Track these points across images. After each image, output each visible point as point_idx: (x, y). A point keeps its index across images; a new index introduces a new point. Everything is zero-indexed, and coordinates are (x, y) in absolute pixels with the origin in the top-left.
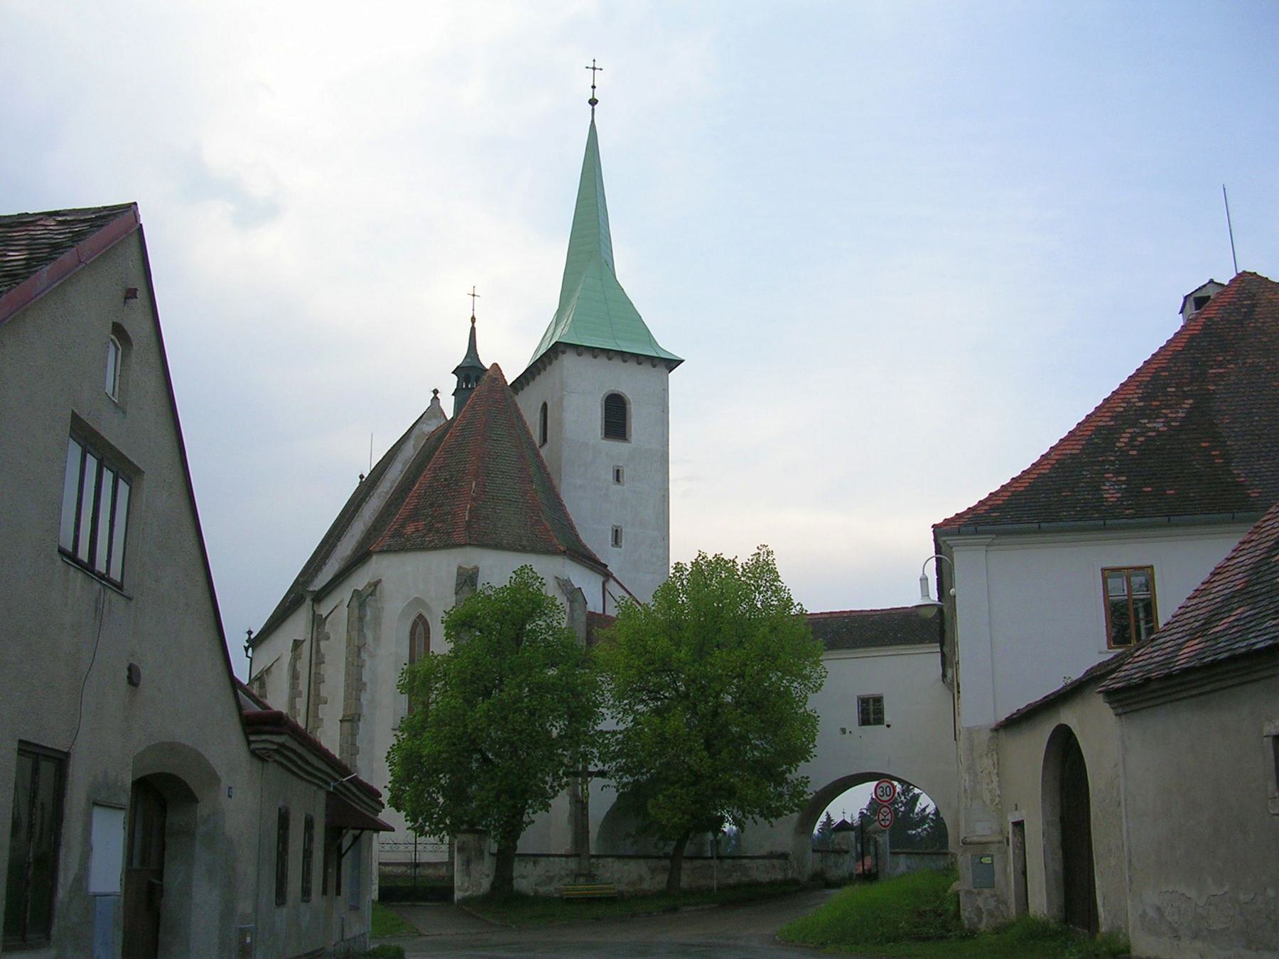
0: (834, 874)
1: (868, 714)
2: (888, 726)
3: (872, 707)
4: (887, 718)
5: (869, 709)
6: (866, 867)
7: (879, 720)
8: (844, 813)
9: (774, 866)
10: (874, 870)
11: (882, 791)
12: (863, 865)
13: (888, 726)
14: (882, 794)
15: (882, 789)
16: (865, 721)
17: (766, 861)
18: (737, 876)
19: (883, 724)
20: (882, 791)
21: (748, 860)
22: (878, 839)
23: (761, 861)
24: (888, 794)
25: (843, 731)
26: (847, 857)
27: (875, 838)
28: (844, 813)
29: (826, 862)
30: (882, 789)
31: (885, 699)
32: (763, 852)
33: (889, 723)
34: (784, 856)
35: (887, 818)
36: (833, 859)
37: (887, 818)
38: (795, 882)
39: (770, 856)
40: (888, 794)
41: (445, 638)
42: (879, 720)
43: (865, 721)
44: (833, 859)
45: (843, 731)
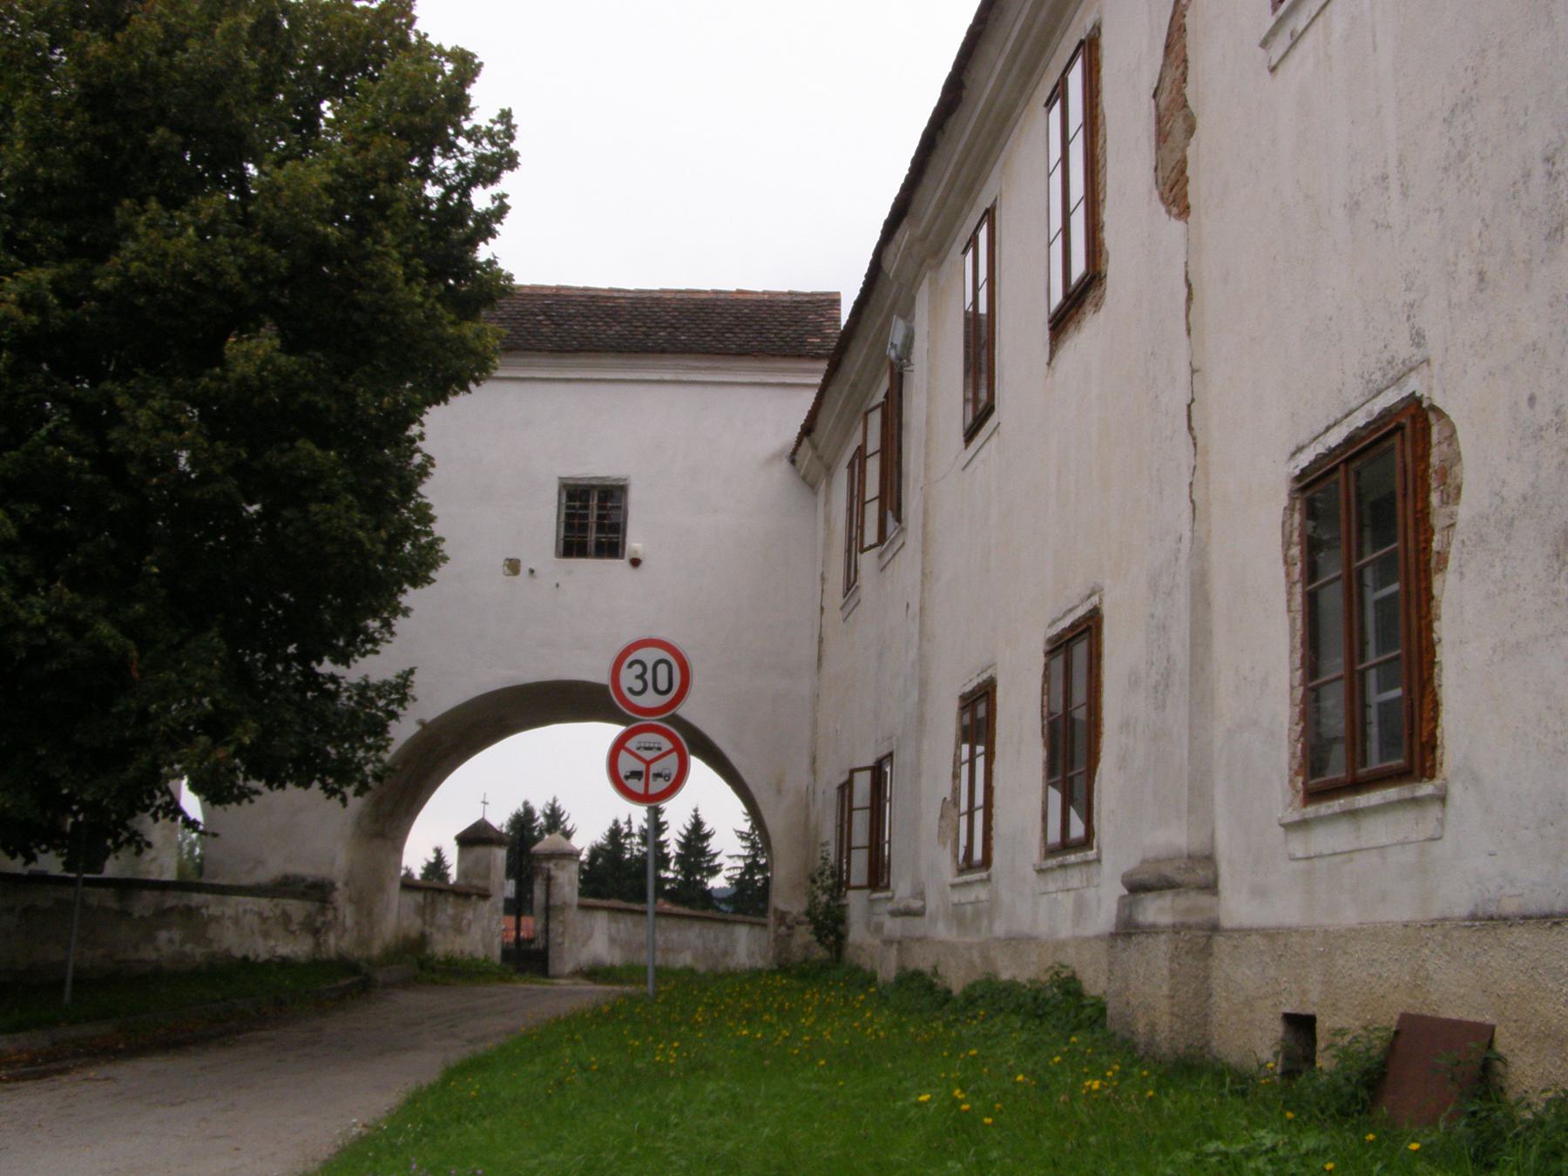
0: (444, 945)
1: (584, 528)
2: (635, 563)
3: (595, 512)
4: (635, 543)
5: (586, 516)
6: (522, 934)
7: (611, 547)
8: (484, 803)
9: (286, 918)
10: (539, 944)
11: (641, 677)
12: (518, 928)
13: (635, 563)
14: (638, 686)
15: (638, 669)
16: (572, 546)
17: (264, 904)
18: (171, 941)
19: (622, 557)
20: (641, 677)
21: (209, 897)
22: (553, 873)
23: (249, 902)
24: (663, 685)
25: (513, 566)
26: (485, 907)
27: (549, 870)
28: (484, 803)
29: (433, 916)
30: (638, 669)
31: (635, 500)
32: (264, 876)
33: (639, 556)
34: (318, 891)
35: (654, 768)
36: (450, 911)
37: (654, 768)
38: (345, 965)
39: (285, 887)
40: (663, 685)
41: (255, 798)
42: (611, 547)
43: (572, 546)
44: (450, 911)
45: (513, 566)
